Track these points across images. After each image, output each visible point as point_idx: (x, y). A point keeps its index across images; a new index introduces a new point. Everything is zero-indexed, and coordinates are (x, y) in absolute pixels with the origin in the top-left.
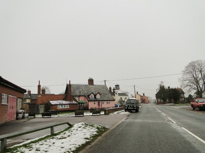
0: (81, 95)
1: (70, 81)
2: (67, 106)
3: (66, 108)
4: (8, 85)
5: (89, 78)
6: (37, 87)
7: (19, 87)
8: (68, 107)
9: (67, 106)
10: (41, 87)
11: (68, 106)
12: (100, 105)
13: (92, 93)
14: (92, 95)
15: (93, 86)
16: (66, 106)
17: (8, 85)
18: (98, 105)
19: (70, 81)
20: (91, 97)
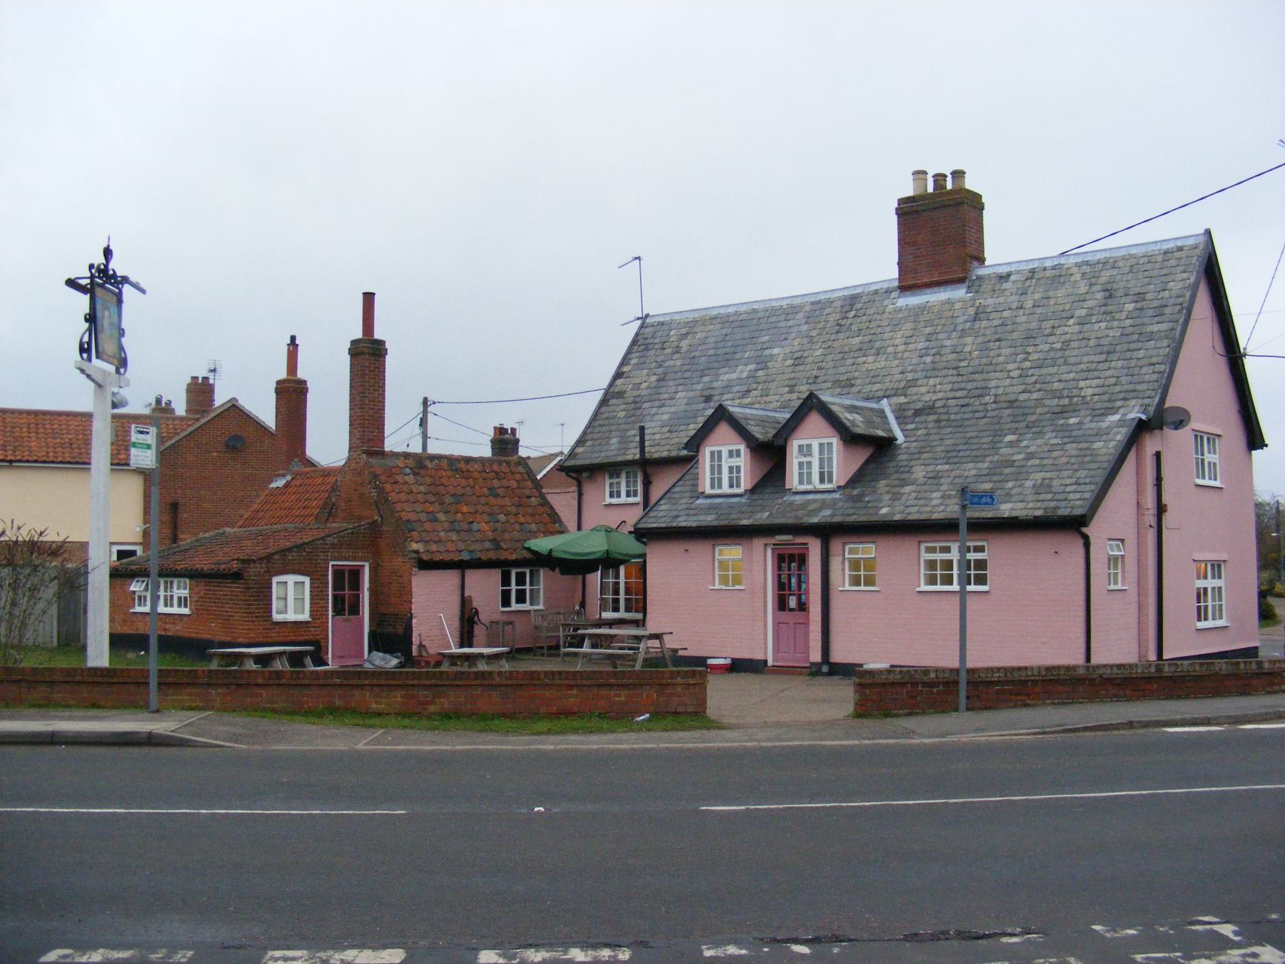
0: (653, 452)
1: (369, 298)
5: (920, 174)
12: (802, 607)
18: (782, 604)
20: (717, 482)
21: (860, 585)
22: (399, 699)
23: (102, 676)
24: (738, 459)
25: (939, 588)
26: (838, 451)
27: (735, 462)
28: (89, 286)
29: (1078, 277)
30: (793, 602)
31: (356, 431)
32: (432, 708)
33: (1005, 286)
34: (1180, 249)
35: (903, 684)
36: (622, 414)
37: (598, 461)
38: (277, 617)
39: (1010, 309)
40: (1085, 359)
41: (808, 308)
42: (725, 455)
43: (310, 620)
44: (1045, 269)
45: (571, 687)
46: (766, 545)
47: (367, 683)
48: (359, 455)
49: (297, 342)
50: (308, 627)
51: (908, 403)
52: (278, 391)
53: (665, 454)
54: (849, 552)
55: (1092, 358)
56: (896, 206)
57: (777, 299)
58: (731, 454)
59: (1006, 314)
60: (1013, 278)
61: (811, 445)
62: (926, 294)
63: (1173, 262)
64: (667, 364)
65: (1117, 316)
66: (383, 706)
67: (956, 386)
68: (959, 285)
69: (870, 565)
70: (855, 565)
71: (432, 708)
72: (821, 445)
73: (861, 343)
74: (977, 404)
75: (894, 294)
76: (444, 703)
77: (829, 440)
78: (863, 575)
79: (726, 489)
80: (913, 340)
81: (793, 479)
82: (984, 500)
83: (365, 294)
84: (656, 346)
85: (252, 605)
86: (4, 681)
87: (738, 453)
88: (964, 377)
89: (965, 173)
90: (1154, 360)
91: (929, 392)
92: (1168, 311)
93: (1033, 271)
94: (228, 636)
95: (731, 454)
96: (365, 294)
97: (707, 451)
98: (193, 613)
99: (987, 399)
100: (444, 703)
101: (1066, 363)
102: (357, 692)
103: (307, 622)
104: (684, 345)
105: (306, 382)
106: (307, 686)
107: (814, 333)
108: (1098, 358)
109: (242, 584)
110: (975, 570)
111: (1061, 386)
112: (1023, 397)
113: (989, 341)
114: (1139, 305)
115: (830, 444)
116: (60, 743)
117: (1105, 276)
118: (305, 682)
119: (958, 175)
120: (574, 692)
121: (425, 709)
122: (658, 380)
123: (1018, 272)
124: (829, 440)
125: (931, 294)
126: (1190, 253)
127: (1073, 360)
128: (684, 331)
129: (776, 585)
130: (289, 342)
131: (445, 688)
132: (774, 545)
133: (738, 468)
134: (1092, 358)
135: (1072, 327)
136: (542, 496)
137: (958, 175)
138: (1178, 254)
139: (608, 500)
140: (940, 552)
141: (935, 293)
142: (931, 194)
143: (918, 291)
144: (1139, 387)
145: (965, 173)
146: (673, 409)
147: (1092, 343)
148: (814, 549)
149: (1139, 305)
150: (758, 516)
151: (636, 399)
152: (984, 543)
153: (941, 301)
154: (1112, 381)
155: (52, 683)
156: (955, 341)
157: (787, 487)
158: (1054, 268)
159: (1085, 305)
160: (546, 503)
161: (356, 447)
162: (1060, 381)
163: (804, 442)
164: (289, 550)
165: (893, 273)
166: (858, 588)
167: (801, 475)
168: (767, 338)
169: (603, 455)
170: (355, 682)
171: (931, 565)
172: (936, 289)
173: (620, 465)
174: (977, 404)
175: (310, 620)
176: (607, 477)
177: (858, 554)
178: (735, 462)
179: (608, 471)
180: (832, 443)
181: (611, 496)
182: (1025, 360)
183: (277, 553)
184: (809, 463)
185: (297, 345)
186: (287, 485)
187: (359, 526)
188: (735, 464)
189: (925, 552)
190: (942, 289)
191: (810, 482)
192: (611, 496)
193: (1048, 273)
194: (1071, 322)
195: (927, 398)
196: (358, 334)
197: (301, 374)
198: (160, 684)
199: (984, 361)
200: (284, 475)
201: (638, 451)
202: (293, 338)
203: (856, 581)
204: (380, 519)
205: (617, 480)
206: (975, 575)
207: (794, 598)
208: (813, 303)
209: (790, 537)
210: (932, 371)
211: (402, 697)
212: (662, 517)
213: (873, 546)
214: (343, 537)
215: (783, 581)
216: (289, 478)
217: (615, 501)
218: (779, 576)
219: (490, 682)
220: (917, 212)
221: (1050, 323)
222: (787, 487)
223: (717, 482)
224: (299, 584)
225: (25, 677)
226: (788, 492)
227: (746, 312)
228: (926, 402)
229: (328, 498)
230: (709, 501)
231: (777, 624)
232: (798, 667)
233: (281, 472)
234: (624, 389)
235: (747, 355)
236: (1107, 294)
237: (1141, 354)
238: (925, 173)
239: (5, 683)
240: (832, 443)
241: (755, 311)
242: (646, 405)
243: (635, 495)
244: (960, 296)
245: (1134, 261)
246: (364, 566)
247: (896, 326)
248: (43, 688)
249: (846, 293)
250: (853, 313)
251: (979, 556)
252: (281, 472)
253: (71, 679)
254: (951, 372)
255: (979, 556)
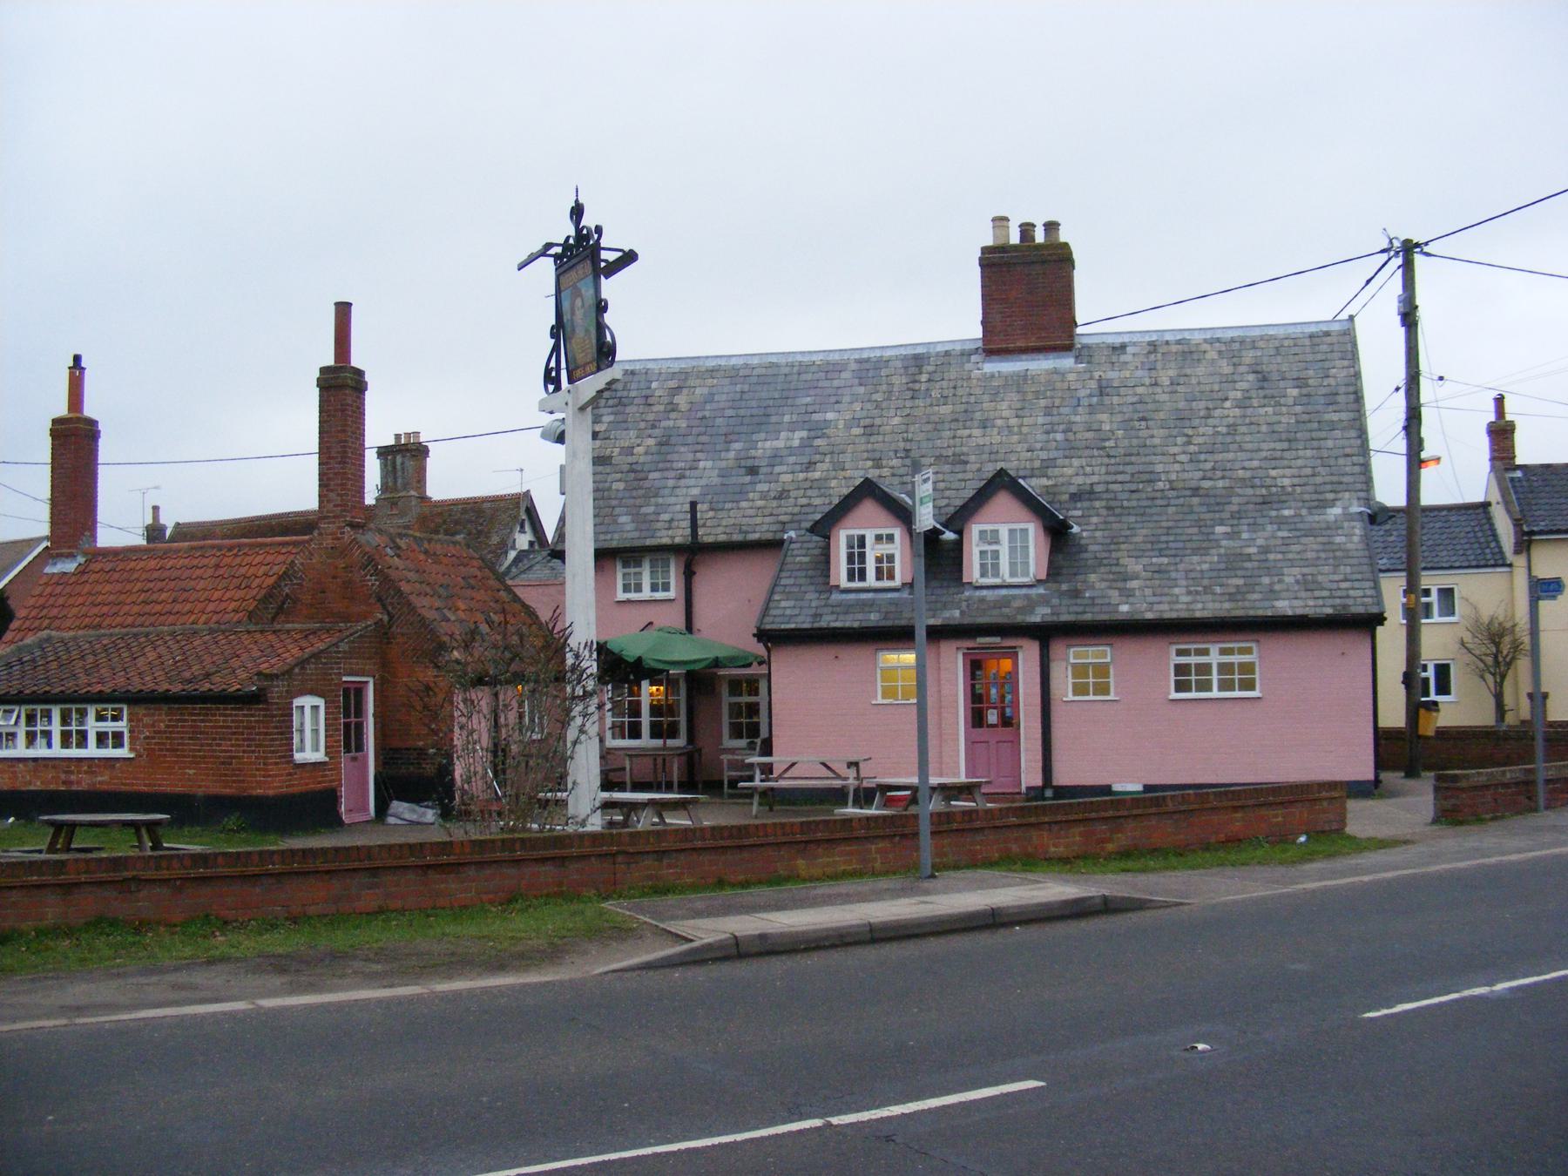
0: (707, 535)
1: (343, 311)
2: (109, 726)
3: (92, 751)
4: (352, 697)
5: (1000, 221)
6: (314, 394)
7: (619, 548)
8: (118, 739)
9: (109, 726)
10: (379, 429)
11: (122, 726)
12: (1008, 722)
13: (868, 490)
14: (868, 524)
15: (1066, 362)
16: (92, 726)
17: (352, 697)
18: (977, 718)
19: (343, 311)
20: (858, 573)
21: (1088, 694)
22: (1078, 838)
23: (731, 836)
24: (890, 546)
25: (1237, 694)
26: (1036, 538)
27: (885, 549)
28: (603, 264)
29: (1212, 355)
30: (992, 717)
31: (332, 495)
32: (1110, 847)
33: (1123, 358)
34: (1327, 334)
35: (1487, 787)
36: (621, 486)
37: (614, 544)
38: (299, 757)
39: (1142, 385)
40: (1264, 446)
41: (854, 366)
42: (869, 541)
43: (327, 759)
44: (1167, 343)
45: (1235, 809)
46: (958, 648)
47: (1046, 819)
48: (339, 528)
49: (83, 365)
50: (325, 770)
51: (1055, 485)
52: (55, 434)
53: (722, 538)
54: (1072, 657)
55: (1272, 445)
56: (979, 255)
57: (802, 353)
58: (879, 538)
59: (1140, 390)
60: (1129, 350)
61: (997, 531)
62: (1022, 360)
63: (1324, 348)
64: (665, 424)
65: (1282, 401)
66: (1061, 849)
67: (1112, 469)
68: (1064, 353)
69: (1102, 670)
70: (1080, 670)
71: (1110, 847)
72: (1011, 531)
73: (952, 412)
74: (1149, 489)
75: (974, 358)
76: (1121, 840)
77: (1022, 526)
78: (1094, 680)
79: (1005, 575)
80: (1026, 412)
81: (973, 570)
82: (1552, 587)
83: (338, 305)
84: (636, 401)
85: (276, 739)
86: (590, 856)
87: (890, 538)
88: (1118, 459)
89: (1059, 225)
90: (1348, 451)
91: (1077, 475)
92: (1341, 399)
93: (1152, 344)
94: (230, 787)
95: (879, 538)
96: (338, 305)
97: (975, 530)
98: (139, 756)
99: (1160, 485)
100: (1121, 840)
101: (1241, 450)
102: (1034, 833)
103: (324, 763)
104: (681, 400)
105: (97, 422)
106: (982, 829)
107: (878, 397)
108: (1279, 446)
109: (260, 710)
110: (1196, 675)
111: (1248, 474)
112: (1206, 484)
113: (1132, 420)
114: (1305, 391)
115: (1025, 531)
116: (1012, 924)
117: (1249, 356)
118: (978, 824)
119: (1051, 227)
120: (1239, 815)
121: (1103, 849)
122: (660, 444)
123: (1134, 344)
124: (1022, 526)
125: (1027, 360)
126: (1341, 339)
127: (1249, 446)
128: (673, 384)
129: (970, 695)
130: (71, 364)
131: (1122, 820)
132: (968, 649)
133: (891, 558)
134: (1272, 445)
135: (1230, 411)
136: (508, 589)
137: (1051, 227)
138: (1328, 340)
139: (621, 596)
140: (1195, 655)
141: (1033, 360)
142: (1015, 246)
143: (1015, 357)
144: (1345, 479)
145: (1059, 225)
146: (703, 482)
147: (1264, 428)
148: (1028, 654)
149: (1305, 391)
150: (947, 614)
151: (634, 466)
152: (1254, 645)
153: (1047, 370)
154: (1308, 471)
155: (661, 854)
156: (1086, 418)
157: (832, 583)
158: (1179, 342)
159: (1240, 385)
160: (516, 599)
161: (335, 517)
162: (1244, 468)
163: (988, 527)
164: (307, 661)
165: (977, 332)
166: (1086, 698)
167: (983, 566)
168: (808, 399)
169: (616, 536)
170: (1033, 820)
171: (1181, 670)
172: (1034, 356)
173: (639, 551)
174: (1149, 489)
175: (327, 759)
176: (619, 566)
177: (1087, 658)
178: (885, 549)
179: (621, 558)
180: (1027, 530)
181: (626, 589)
182: (1189, 443)
183: (296, 665)
184: (996, 554)
185: (84, 369)
186: (82, 571)
187: (366, 627)
188: (885, 552)
189: (1170, 654)
190: (1041, 356)
191: (996, 574)
192: (626, 589)
193: (1174, 348)
194: (1228, 404)
195: (1080, 480)
196: (330, 361)
197: (89, 411)
198: (933, 833)
199: (1135, 442)
200: (72, 556)
201: (688, 531)
202: (77, 359)
203: (1080, 689)
204: (386, 618)
205: (637, 570)
206: (1240, 679)
207: (995, 711)
208: (859, 361)
209: (997, 640)
210: (1071, 450)
211: (1081, 834)
212: (792, 613)
213: (1108, 649)
214: (353, 642)
215: (978, 692)
216: (81, 559)
217: (633, 596)
218: (973, 686)
219: (1164, 809)
220: (1008, 264)
221: (1202, 405)
222: (965, 580)
223: (858, 573)
224: (315, 708)
225: (624, 848)
226: (967, 586)
227: (760, 366)
228: (1079, 485)
229: (274, 587)
230: (844, 596)
231: (971, 744)
232: (998, 794)
233: (65, 551)
234: (608, 452)
235: (787, 418)
236: (1260, 376)
237: (1330, 443)
238: (1006, 219)
239: (593, 859)
240: (1027, 530)
241: (777, 365)
242: (652, 476)
243: (666, 588)
244: (1068, 366)
245: (1277, 344)
246: (367, 682)
247: (995, 396)
248: (649, 862)
249: (911, 351)
250: (924, 378)
251: (1246, 658)
252: (65, 551)
253: (688, 845)
254: (1096, 452)
255: (1246, 658)
